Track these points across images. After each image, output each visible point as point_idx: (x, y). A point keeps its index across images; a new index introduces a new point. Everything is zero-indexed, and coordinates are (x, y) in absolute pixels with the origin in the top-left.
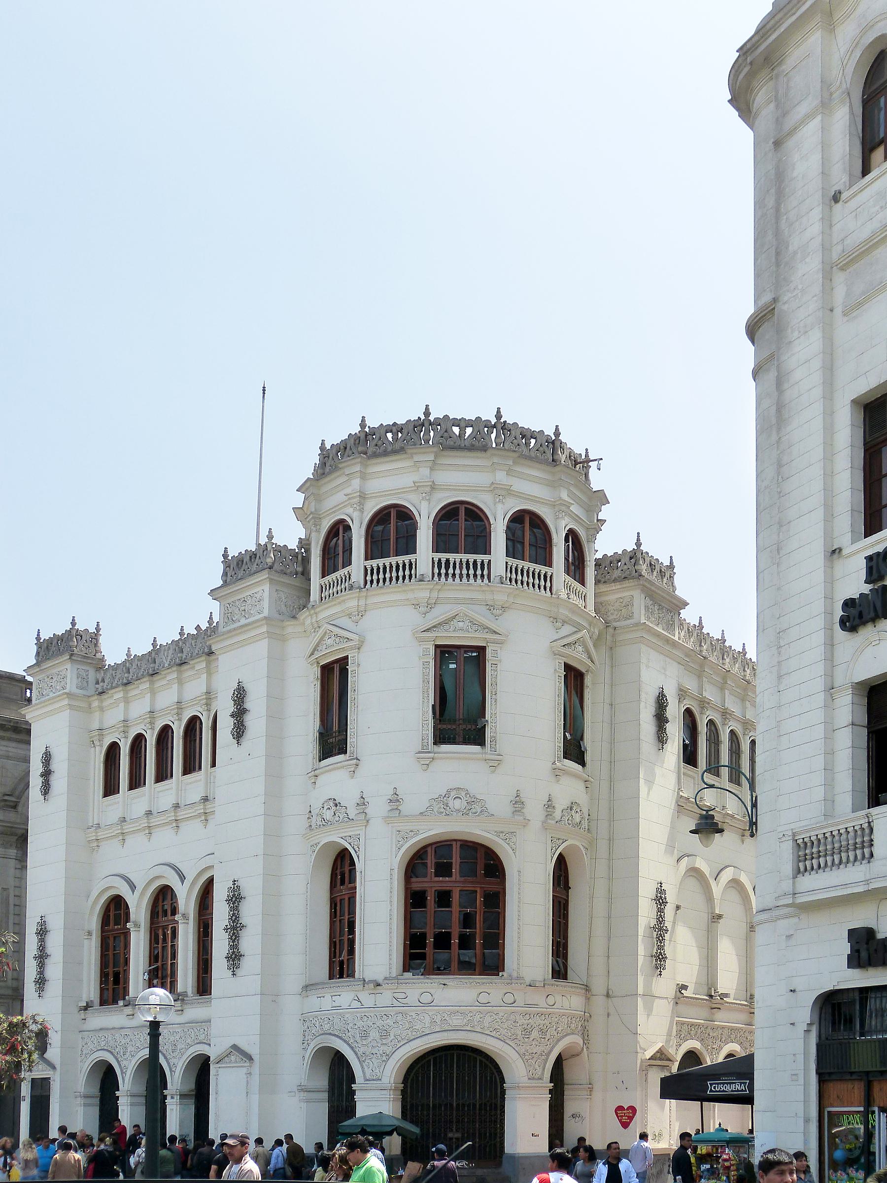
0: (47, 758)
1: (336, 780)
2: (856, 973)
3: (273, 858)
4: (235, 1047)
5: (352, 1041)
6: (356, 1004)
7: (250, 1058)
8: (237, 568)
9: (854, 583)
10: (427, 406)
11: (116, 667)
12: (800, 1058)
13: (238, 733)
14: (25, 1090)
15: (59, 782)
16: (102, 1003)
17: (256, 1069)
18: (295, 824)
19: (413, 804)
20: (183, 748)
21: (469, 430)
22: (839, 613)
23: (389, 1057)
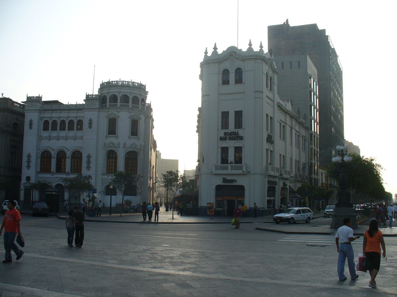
1: (112, 139)
16: (41, 172)
19: (127, 146)
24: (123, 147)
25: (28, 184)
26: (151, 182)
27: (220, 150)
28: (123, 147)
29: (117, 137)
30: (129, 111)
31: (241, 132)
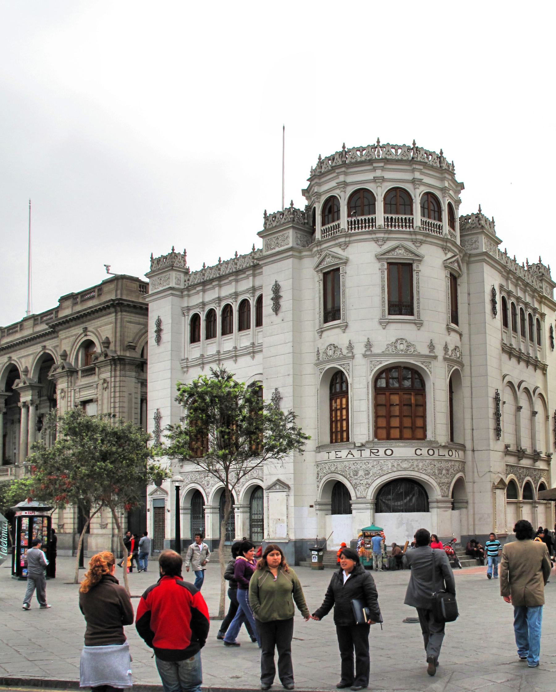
0: (159, 323)
1: (334, 336)
3: (297, 376)
4: (278, 480)
5: (348, 476)
7: (289, 487)
10: (414, 140)
11: (196, 273)
13: (276, 309)
14: (149, 505)
15: (166, 336)
17: (292, 493)
18: (310, 358)
20: (246, 315)
23: (370, 485)
24: (365, 356)
28: (365, 356)
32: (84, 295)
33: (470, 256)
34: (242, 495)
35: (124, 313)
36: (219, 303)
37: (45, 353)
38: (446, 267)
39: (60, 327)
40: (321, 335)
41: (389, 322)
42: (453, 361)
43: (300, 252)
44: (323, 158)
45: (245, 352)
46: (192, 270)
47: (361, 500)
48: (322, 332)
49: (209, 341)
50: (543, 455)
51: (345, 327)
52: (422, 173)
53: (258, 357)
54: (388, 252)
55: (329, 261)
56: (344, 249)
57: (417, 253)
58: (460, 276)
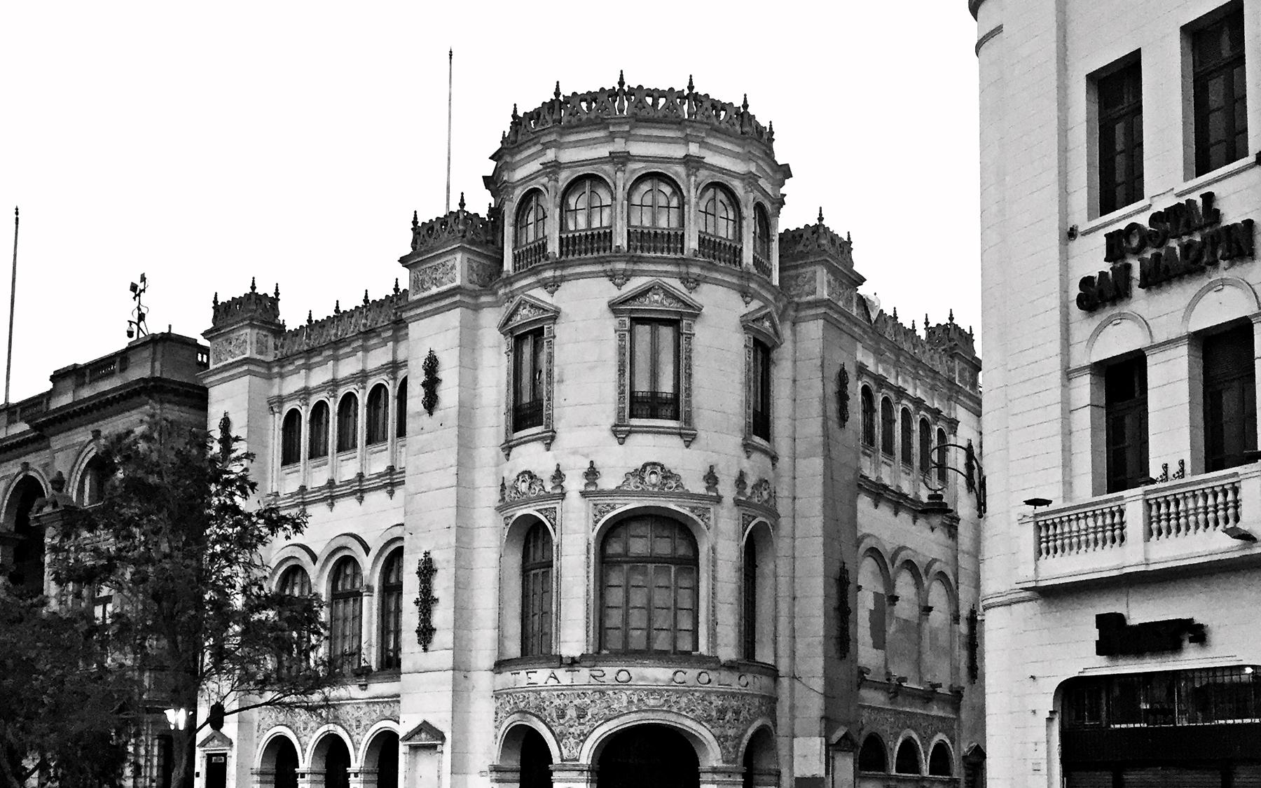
2: (1102, 660)
3: (463, 532)
6: (552, 682)
8: (424, 234)
9: (1092, 259)
11: (296, 333)
12: (1043, 747)
14: (200, 766)
18: (487, 496)
20: (378, 414)
21: (662, 101)
22: (1075, 291)
23: (586, 736)
24: (584, 494)
25: (423, 735)
26: (172, 727)
27: (1084, 389)
28: (584, 494)
29: (549, 440)
30: (608, 267)
31: (1239, 196)
32: (101, 368)
33: (798, 307)
34: (363, 748)
35: (167, 405)
36: (334, 391)
37: (27, 478)
38: (746, 328)
39: (52, 429)
40: (508, 455)
41: (630, 432)
42: (755, 506)
43: (477, 297)
44: (520, 114)
45: (378, 483)
46: (291, 325)
47: (570, 765)
48: (511, 448)
49: (288, 469)
50: (943, 690)
51: (549, 440)
52: (703, 144)
53: (399, 492)
54: (634, 298)
55: (525, 314)
56: (552, 293)
57: (689, 301)
58: (776, 345)
